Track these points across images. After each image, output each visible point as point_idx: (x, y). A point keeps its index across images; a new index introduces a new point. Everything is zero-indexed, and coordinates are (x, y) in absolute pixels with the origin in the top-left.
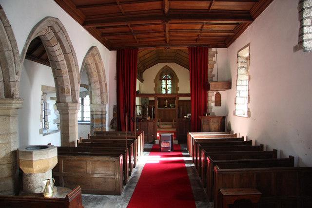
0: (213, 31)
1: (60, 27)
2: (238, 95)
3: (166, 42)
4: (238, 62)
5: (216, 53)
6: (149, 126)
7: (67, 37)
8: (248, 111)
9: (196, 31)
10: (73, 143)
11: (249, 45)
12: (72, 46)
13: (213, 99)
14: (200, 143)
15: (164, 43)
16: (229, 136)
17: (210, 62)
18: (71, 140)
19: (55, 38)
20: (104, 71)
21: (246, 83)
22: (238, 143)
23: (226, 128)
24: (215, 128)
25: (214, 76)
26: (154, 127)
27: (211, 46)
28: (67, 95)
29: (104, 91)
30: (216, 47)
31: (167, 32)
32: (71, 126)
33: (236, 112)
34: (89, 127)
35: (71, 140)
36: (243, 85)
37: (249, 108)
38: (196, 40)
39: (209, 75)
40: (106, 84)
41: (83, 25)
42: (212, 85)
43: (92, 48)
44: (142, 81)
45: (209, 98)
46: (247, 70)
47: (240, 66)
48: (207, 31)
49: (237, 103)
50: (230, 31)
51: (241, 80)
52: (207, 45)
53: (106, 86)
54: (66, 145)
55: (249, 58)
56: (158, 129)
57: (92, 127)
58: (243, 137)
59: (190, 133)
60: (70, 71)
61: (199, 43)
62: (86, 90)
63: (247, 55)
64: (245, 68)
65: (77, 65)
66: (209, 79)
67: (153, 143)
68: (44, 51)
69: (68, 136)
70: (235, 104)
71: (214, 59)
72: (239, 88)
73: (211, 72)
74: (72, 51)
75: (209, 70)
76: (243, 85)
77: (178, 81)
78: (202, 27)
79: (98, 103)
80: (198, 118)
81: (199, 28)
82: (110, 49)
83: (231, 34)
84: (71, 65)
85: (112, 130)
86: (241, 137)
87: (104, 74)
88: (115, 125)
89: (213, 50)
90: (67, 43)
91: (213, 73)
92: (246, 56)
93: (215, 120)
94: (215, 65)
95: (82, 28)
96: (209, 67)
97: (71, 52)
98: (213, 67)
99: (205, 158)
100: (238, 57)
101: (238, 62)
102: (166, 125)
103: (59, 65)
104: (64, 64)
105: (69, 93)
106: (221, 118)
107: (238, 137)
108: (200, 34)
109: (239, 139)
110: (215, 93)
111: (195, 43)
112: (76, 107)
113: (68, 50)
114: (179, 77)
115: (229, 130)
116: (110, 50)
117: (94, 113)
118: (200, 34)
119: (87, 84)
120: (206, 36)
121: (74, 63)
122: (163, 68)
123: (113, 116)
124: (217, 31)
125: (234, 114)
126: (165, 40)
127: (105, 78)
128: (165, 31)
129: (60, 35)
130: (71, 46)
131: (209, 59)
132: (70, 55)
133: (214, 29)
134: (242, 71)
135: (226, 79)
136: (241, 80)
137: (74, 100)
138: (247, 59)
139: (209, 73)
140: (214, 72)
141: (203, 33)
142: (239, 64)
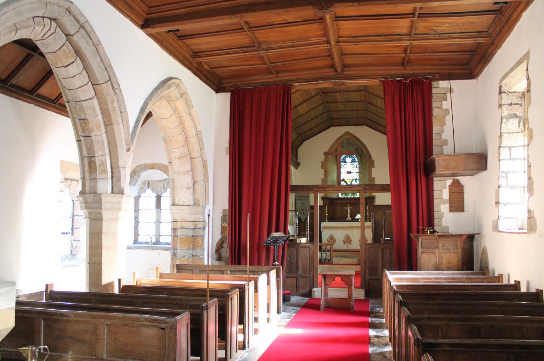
0: (440, 36)
1: (77, 21)
2: (502, 181)
3: (336, 71)
4: (500, 106)
5: (451, 90)
6: (301, 255)
7: (97, 47)
8: (529, 218)
9: (399, 37)
10: (111, 285)
11: (526, 57)
12: (110, 66)
13: (446, 194)
14: (401, 294)
15: (330, 72)
16: (482, 280)
17: (435, 112)
18: (105, 280)
19: (68, 48)
20: (198, 134)
21: (520, 153)
22: (349, 185)
23: (476, 265)
24: (448, 263)
25: (446, 143)
26: (312, 261)
27: (438, 77)
28: (101, 176)
29: (200, 177)
30: (450, 77)
31: (333, 42)
32: (107, 248)
33: (500, 222)
34: (168, 255)
35: (105, 280)
36: (514, 159)
37: (531, 209)
38: (403, 63)
39: (435, 142)
40: (204, 163)
41: (143, 27)
42: (440, 163)
43: (166, 82)
44: (297, 165)
45: (436, 194)
46: (525, 121)
47: (506, 113)
48: (425, 36)
49: (501, 200)
50: (480, 34)
51: (510, 148)
52: (430, 74)
53: (205, 167)
54: (94, 290)
55: (526, 95)
56: (322, 269)
57: (174, 255)
58: (519, 282)
59: (388, 272)
60: (108, 124)
61: (409, 70)
62: (165, 176)
63: (522, 86)
64: (520, 118)
65: (123, 112)
66: (435, 150)
67: (309, 294)
68: (49, 73)
69: (100, 274)
70: (498, 203)
71: (446, 105)
72: (505, 166)
73: (440, 134)
74: (111, 80)
75: (435, 130)
76: (514, 159)
77: (373, 166)
78: (411, 27)
79: (187, 203)
80: (409, 237)
81: (405, 31)
82: (218, 90)
83: (480, 40)
84: (111, 109)
85: (217, 263)
86: (512, 282)
87: (200, 141)
88: (226, 252)
89: (443, 84)
90: (99, 59)
91: (444, 136)
92: (521, 90)
93: (449, 244)
94: (448, 119)
95: (140, 34)
96: (435, 122)
97: (110, 80)
98: (443, 124)
99: (407, 333)
100: (501, 92)
101: (500, 106)
102: (347, 257)
103: (82, 109)
104: (93, 108)
105: (105, 171)
106: (464, 237)
107: (505, 282)
108: (408, 43)
109: (508, 286)
110: (449, 182)
111: (400, 70)
112: (120, 203)
113: (101, 76)
114: (374, 157)
115: (484, 269)
116: (217, 91)
117: (179, 225)
118: (408, 43)
119: (165, 162)
120: (424, 50)
121: (116, 105)
122: (341, 137)
123: (222, 233)
124: (450, 35)
125: (496, 227)
126: (333, 66)
127: (202, 149)
128: (328, 42)
129: (80, 39)
130: (108, 68)
131: (435, 104)
132: (106, 88)
133: (440, 29)
134: (513, 125)
135: (475, 149)
136: (510, 148)
137: (115, 189)
138: (523, 96)
139: (434, 136)
140: (447, 135)
141: (415, 43)
142: (504, 108)
